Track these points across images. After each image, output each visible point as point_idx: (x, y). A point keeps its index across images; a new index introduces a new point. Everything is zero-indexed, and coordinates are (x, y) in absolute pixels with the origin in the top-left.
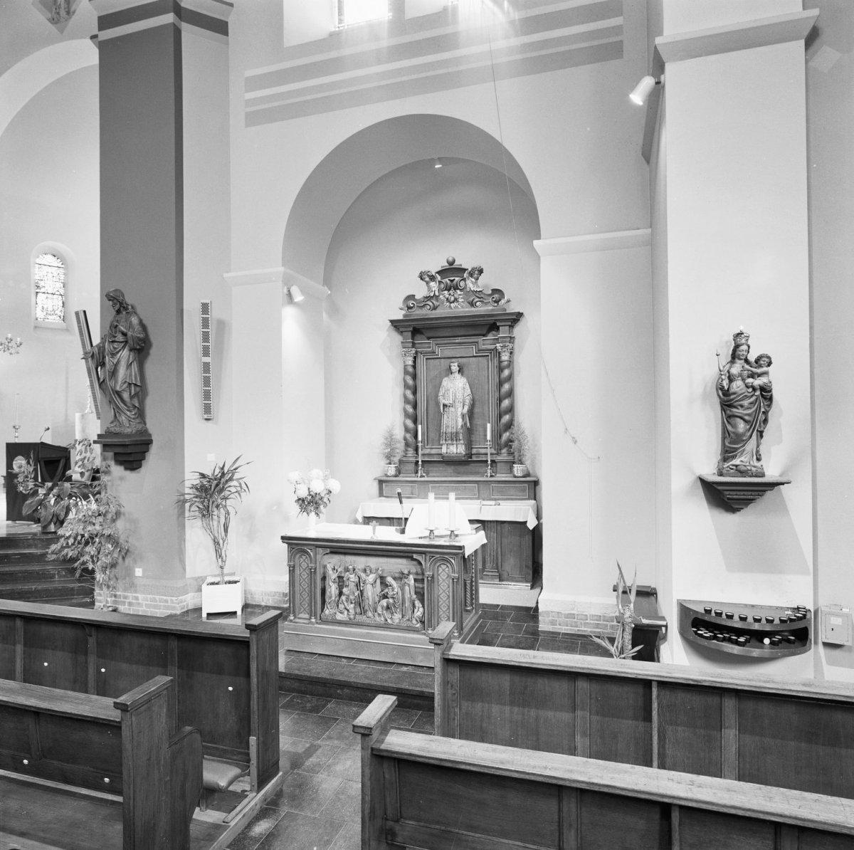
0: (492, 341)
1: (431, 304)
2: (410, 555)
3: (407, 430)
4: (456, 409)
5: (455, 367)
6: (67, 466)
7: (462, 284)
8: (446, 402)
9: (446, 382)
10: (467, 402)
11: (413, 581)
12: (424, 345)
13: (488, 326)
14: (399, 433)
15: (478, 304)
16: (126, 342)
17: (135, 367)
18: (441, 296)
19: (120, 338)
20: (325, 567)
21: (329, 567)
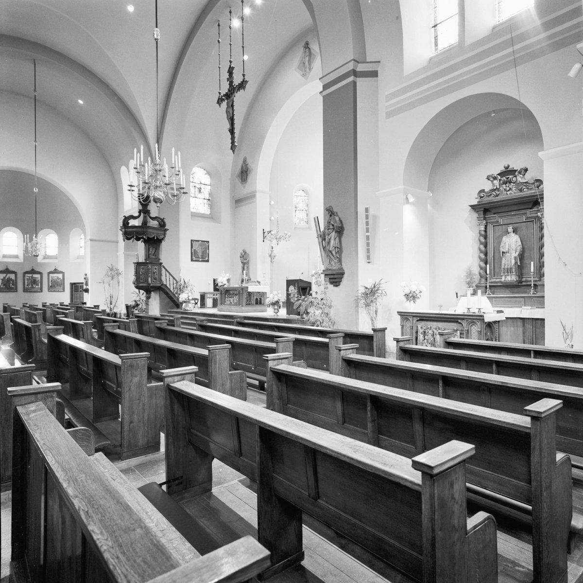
0: (535, 212)
1: (494, 193)
2: (457, 320)
3: (481, 268)
4: (511, 254)
5: (510, 229)
6: (310, 289)
7: (514, 179)
8: (504, 251)
9: (504, 239)
10: (519, 249)
11: (459, 334)
12: (491, 218)
13: (532, 203)
14: (476, 270)
15: (525, 190)
16: (334, 229)
17: (337, 239)
18: (501, 188)
19: (331, 227)
20: (417, 327)
21: (419, 327)
